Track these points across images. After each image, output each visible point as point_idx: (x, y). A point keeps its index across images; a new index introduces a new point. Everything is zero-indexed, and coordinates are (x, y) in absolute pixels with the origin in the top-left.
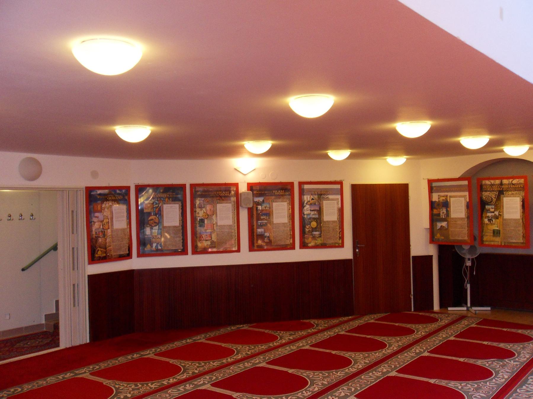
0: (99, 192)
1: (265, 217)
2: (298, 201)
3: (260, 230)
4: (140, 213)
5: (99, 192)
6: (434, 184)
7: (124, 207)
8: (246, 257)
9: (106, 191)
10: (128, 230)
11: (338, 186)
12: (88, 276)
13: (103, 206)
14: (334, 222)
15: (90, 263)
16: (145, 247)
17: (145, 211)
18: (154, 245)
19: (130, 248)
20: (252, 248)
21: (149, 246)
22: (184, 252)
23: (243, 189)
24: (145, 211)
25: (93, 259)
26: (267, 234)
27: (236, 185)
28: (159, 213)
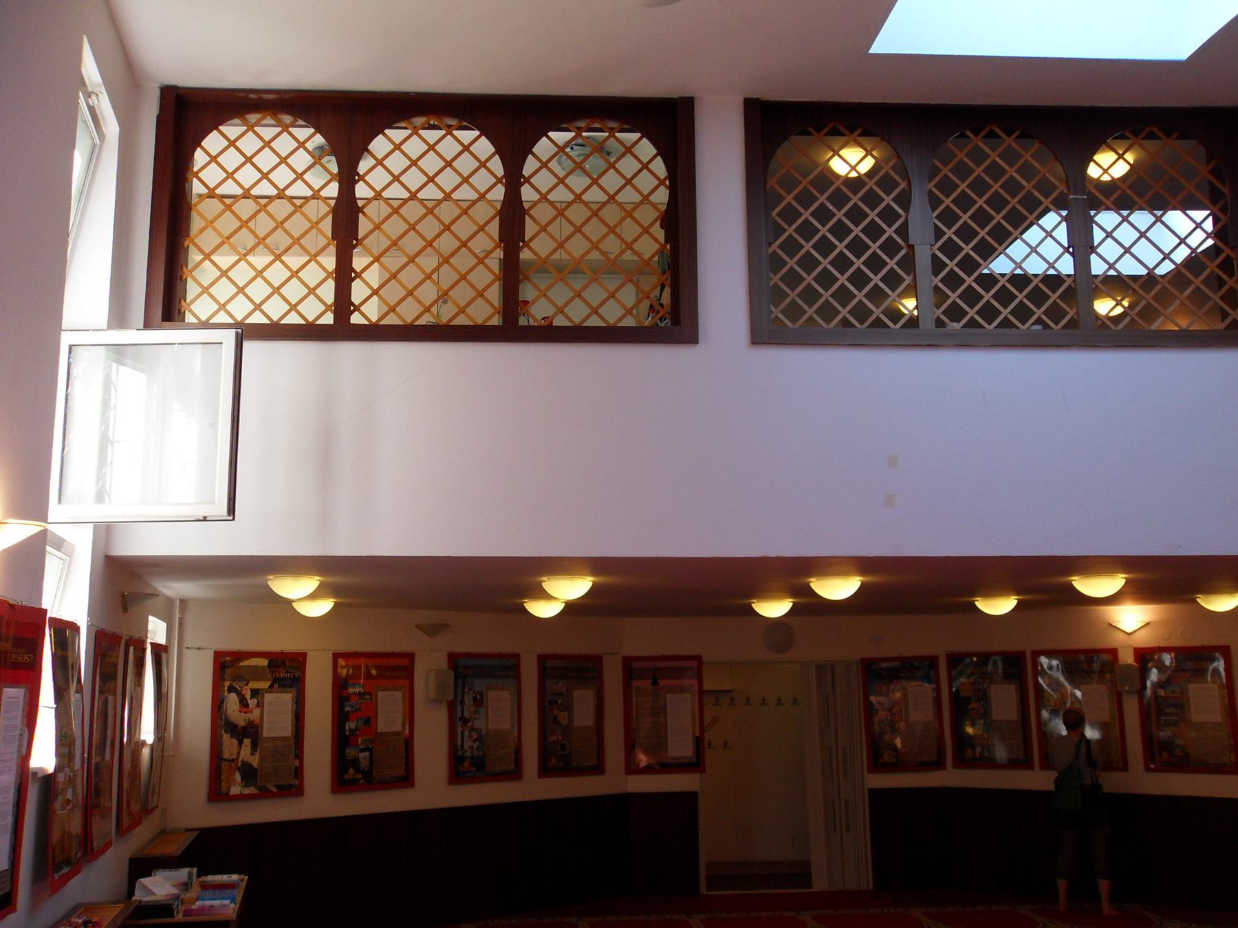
0: (884, 665)
1: (1172, 710)
2: (535, 694)
3: (1165, 734)
4: (956, 698)
5: (884, 665)
6: (549, 663)
7: (928, 688)
8: (533, 787)
9: (896, 664)
10: (516, 734)
11: (694, 664)
12: (870, 790)
13: (892, 687)
14: (285, 738)
15: (871, 771)
16: (967, 754)
17: (963, 695)
18: (978, 749)
19: (941, 751)
20: (545, 771)
21: (969, 751)
22: (939, 764)
23: (1127, 658)
24: (963, 695)
25: (876, 765)
26: (1179, 742)
27: (1113, 652)
28: (984, 697)
